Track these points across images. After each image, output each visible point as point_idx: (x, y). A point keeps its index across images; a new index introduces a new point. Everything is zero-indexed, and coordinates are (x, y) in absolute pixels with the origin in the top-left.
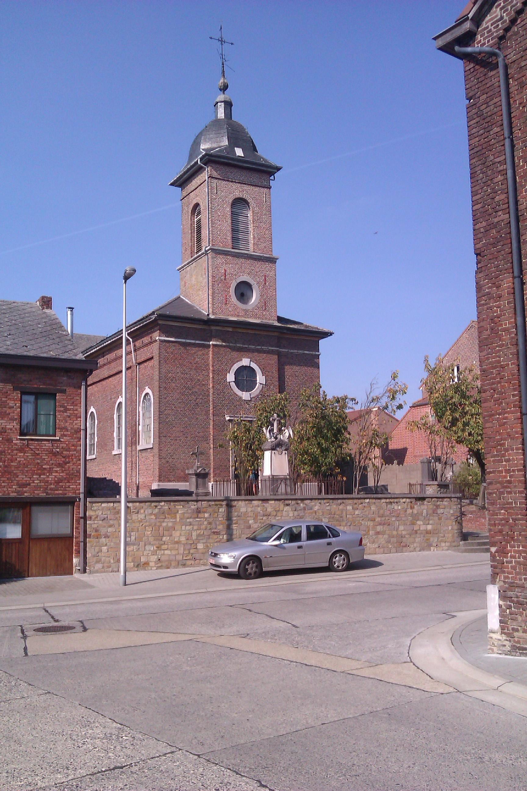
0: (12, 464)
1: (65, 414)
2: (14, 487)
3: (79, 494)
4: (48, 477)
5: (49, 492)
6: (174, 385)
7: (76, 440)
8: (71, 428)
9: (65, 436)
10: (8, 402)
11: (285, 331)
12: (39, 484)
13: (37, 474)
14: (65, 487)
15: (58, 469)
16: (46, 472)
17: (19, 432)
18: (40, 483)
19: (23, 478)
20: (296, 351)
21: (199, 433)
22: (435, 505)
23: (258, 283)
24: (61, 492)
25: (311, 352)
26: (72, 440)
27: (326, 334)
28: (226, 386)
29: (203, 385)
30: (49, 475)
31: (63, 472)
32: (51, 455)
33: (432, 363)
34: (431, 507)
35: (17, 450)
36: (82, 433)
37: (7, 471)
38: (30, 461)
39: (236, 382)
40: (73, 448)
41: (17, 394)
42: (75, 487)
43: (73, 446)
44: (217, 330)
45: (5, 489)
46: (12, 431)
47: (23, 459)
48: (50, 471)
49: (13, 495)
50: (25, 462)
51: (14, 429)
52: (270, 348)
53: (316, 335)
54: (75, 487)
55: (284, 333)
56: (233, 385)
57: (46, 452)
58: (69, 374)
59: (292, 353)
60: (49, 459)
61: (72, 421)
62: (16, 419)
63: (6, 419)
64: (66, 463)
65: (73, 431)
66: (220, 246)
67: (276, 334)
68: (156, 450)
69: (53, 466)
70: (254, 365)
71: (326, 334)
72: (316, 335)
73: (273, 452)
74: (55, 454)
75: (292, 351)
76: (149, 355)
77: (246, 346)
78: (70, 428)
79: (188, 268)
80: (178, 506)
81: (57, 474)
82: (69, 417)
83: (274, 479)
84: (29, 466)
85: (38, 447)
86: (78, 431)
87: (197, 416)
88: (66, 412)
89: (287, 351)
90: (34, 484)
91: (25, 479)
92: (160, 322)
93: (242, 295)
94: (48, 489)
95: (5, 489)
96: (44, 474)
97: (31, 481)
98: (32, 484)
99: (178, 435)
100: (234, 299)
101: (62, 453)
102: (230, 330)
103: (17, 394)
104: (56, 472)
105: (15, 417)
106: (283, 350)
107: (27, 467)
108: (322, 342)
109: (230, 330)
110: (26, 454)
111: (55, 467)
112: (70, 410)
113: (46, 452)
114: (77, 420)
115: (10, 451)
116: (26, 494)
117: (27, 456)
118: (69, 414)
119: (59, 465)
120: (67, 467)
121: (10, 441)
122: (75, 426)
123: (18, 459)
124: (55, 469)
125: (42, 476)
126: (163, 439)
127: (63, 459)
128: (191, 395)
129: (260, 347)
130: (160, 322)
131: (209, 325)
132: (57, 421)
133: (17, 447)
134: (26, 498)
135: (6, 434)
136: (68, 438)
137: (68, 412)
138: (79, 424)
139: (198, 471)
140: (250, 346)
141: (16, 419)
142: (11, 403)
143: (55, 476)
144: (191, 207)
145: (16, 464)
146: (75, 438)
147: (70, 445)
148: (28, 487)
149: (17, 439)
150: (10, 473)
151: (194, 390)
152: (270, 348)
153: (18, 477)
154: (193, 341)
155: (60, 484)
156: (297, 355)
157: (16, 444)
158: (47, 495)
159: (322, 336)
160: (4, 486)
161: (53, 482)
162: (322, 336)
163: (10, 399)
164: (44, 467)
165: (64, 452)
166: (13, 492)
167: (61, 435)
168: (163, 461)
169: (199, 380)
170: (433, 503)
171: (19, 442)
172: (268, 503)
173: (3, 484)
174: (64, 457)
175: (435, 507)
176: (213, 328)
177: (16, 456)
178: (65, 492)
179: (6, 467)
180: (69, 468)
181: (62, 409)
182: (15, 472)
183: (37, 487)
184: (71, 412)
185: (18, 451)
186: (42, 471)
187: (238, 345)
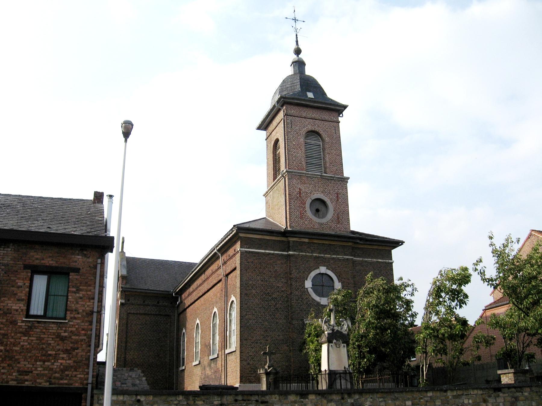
0: (14, 348)
1: (77, 295)
2: (14, 374)
3: (87, 384)
4: (53, 364)
5: (53, 381)
6: (254, 291)
7: (87, 324)
8: (83, 311)
9: (75, 318)
10: (17, 281)
11: (359, 241)
12: (42, 372)
13: (40, 361)
14: (71, 376)
15: (65, 356)
16: (51, 358)
17: (25, 313)
18: (44, 370)
19: (24, 365)
20: (370, 260)
21: (279, 336)
22: (512, 397)
23: (331, 200)
24: (66, 382)
25: (385, 261)
26: (83, 324)
27: (397, 243)
28: (304, 292)
29: (282, 291)
30: (55, 362)
31: (70, 359)
32: (58, 339)
33: (499, 243)
34: (509, 399)
35: (20, 333)
36: (95, 315)
37: (9, 357)
38: (35, 346)
39: (314, 286)
40: (83, 332)
41: (27, 272)
42: (82, 376)
43: (83, 330)
44: (294, 241)
45: (4, 377)
46: (18, 313)
47: (26, 344)
48: (56, 357)
49: (13, 383)
50: (28, 346)
51: (20, 310)
52: (344, 257)
53: (388, 245)
54: (82, 376)
55: (357, 243)
56: (310, 291)
57: (53, 336)
58: (85, 252)
59: (366, 261)
60: (56, 344)
61: (84, 303)
62: (23, 300)
63: (12, 299)
64: (74, 349)
65: (85, 314)
66: (295, 169)
67: (350, 244)
68: (238, 353)
69: (59, 352)
70: (330, 273)
71: (397, 243)
72: (388, 245)
73: (330, 344)
74: (63, 339)
75: (366, 259)
76: (233, 267)
77: (323, 255)
78: (81, 311)
79: (271, 193)
80: (198, 401)
81: (63, 361)
82: (81, 298)
83: (332, 375)
84: (33, 352)
85: (44, 331)
86: (92, 312)
87: (277, 321)
88: (78, 293)
89: (361, 259)
90: (37, 372)
91: (27, 366)
92: (241, 235)
93: (317, 210)
94: (52, 377)
95: (4, 377)
96: (48, 361)
97: (33, 369)
98: (34, 372)
99: (258, 338)
100: (309, 214)
101: (70, 337)
102: (306, 240)
103: (27, 272)
104: (63, 359)
105: (23, 298)
106: (358, 259)
107: (30, 352)
108: (394, 252)
109: (306, 240)
110: (30, 338)
111: (62, 353)
112: (82, 290)
113: (53, 336)
114: (89, 301)
115: (13, 335)
116: (26, 383)
117: (32, 340)
118: (81, 295)
119: (66, 351)
120: (74, 353)
121: (14, 323)
122: (87, 309)
123: (21, 343)
124: (61, 356)
125: (46, 363)
126: (245, 342)
127: (71, 345)
128: (271, 300)
129: (335, 256)
130: (241, 235)
131: (287, 237)
132: (69, 303)
133: (21, 330)
134: (27, 387)
135: (11, 315)
136: (79, 321)
137: (81, 292)
138: (92, 306)
139: (269, 371)
140: (326, 256)
141: (23, 300)
142: (20, 283)
143: (61, 364)
144: (273, 143)
145: (18, 349)
146: (87, 321)
147: (80, 329)
148: (30, 374)
149: (23, 321)
150: (11, 358)
151: (274, 296)
152: (344, 257)
153: (19, 363)
154: (272, 252)
155: (66, 373)
156: (371, 263)
157: (20, 327)
158: (50, 384)
159: (394, 245)
160: (3, 374)
161: (58, 370)
162: (394, 245)
163: (19, 279)
164: (49, 352)
165: (73, 337)
166: (13, 380)
167: (71, 318)
168: (245, 363)
169: (278, 287)
170: (511, 394)
171: (24, 324)
172: (308, 398)
173: (2, 371)
174: (72, 343)
175: (513, 399)
176: (291, 239)
177: (20, 340)
178: (71, 382)
179: (8, 351)
180: (77, 354)
181: (74, 289)
182: (17, 357)
183: (39, 376)
184: (83, 293)
185: (22, 335)
186: (47, 357)
187: (314, 255)
